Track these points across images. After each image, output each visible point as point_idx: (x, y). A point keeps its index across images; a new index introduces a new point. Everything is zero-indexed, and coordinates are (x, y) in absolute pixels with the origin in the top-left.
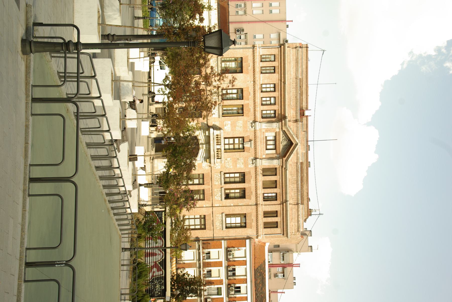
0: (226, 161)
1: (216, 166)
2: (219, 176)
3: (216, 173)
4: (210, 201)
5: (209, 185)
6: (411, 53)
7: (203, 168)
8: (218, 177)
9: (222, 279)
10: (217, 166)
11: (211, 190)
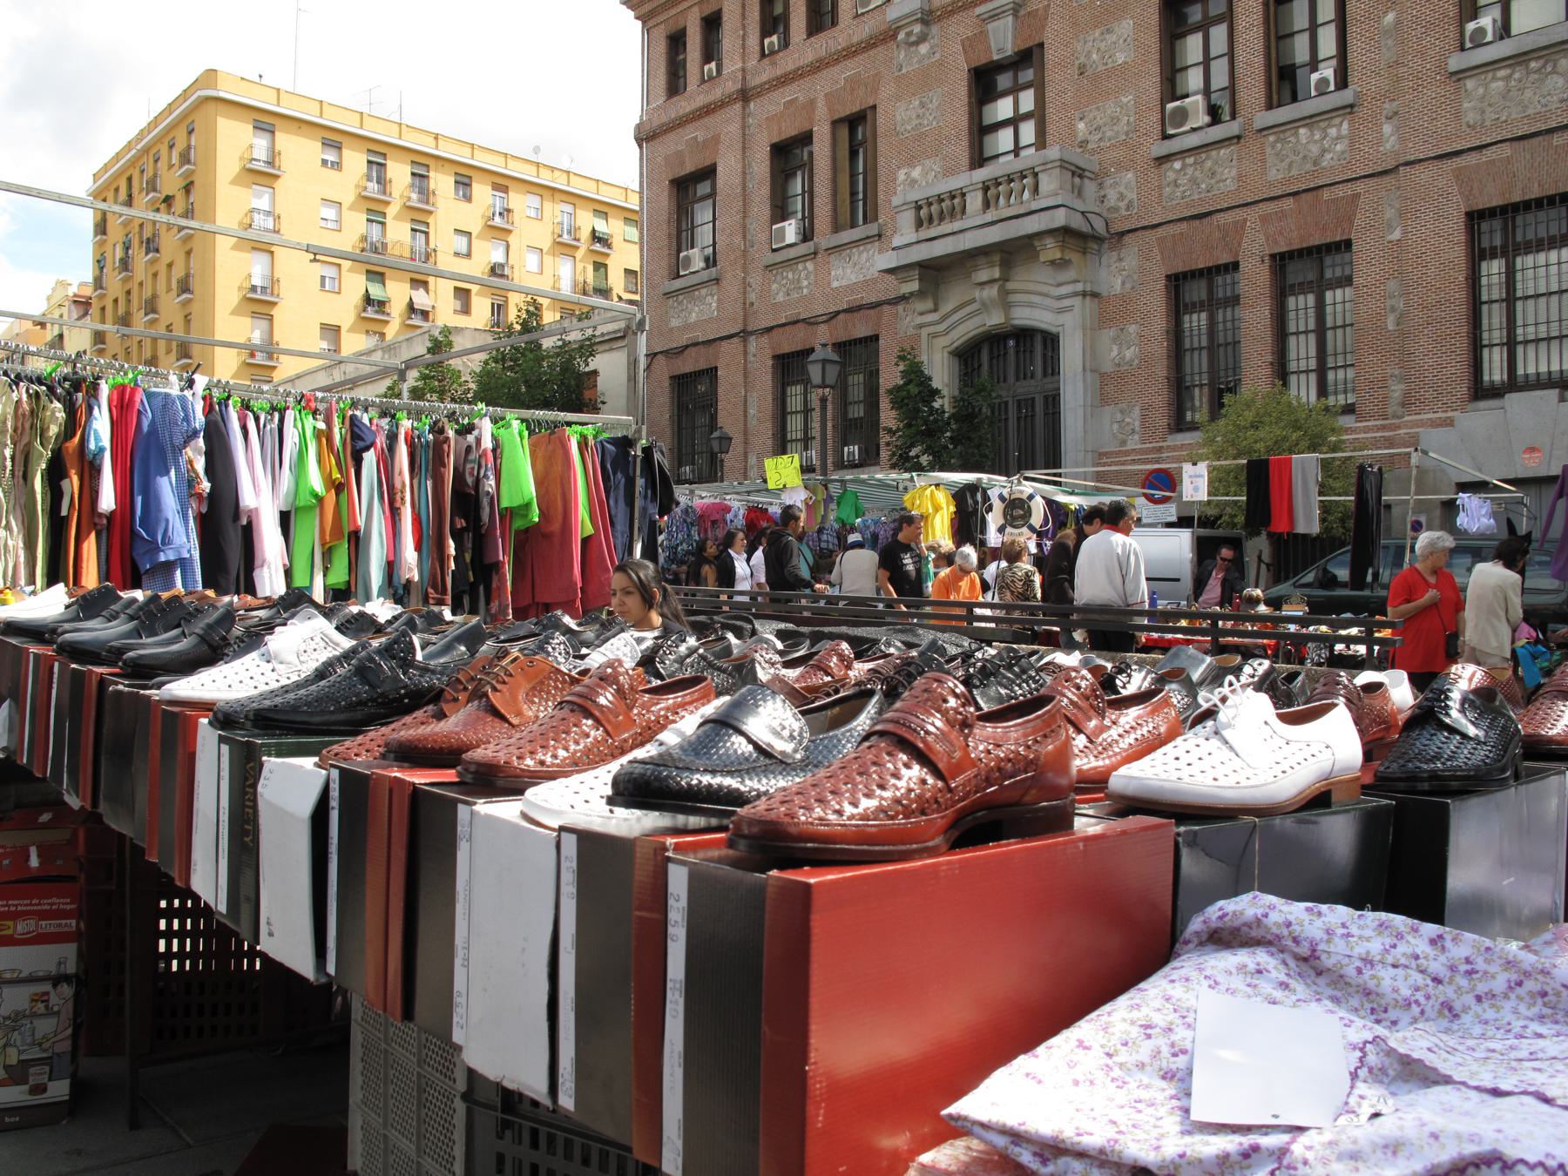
0: (1090, 146)
1: (1122, 204)
5: (1240, 227)
7: (1128, 286)
8: (1190, 171)
10: (1121, 197)
11: (1270, 207)
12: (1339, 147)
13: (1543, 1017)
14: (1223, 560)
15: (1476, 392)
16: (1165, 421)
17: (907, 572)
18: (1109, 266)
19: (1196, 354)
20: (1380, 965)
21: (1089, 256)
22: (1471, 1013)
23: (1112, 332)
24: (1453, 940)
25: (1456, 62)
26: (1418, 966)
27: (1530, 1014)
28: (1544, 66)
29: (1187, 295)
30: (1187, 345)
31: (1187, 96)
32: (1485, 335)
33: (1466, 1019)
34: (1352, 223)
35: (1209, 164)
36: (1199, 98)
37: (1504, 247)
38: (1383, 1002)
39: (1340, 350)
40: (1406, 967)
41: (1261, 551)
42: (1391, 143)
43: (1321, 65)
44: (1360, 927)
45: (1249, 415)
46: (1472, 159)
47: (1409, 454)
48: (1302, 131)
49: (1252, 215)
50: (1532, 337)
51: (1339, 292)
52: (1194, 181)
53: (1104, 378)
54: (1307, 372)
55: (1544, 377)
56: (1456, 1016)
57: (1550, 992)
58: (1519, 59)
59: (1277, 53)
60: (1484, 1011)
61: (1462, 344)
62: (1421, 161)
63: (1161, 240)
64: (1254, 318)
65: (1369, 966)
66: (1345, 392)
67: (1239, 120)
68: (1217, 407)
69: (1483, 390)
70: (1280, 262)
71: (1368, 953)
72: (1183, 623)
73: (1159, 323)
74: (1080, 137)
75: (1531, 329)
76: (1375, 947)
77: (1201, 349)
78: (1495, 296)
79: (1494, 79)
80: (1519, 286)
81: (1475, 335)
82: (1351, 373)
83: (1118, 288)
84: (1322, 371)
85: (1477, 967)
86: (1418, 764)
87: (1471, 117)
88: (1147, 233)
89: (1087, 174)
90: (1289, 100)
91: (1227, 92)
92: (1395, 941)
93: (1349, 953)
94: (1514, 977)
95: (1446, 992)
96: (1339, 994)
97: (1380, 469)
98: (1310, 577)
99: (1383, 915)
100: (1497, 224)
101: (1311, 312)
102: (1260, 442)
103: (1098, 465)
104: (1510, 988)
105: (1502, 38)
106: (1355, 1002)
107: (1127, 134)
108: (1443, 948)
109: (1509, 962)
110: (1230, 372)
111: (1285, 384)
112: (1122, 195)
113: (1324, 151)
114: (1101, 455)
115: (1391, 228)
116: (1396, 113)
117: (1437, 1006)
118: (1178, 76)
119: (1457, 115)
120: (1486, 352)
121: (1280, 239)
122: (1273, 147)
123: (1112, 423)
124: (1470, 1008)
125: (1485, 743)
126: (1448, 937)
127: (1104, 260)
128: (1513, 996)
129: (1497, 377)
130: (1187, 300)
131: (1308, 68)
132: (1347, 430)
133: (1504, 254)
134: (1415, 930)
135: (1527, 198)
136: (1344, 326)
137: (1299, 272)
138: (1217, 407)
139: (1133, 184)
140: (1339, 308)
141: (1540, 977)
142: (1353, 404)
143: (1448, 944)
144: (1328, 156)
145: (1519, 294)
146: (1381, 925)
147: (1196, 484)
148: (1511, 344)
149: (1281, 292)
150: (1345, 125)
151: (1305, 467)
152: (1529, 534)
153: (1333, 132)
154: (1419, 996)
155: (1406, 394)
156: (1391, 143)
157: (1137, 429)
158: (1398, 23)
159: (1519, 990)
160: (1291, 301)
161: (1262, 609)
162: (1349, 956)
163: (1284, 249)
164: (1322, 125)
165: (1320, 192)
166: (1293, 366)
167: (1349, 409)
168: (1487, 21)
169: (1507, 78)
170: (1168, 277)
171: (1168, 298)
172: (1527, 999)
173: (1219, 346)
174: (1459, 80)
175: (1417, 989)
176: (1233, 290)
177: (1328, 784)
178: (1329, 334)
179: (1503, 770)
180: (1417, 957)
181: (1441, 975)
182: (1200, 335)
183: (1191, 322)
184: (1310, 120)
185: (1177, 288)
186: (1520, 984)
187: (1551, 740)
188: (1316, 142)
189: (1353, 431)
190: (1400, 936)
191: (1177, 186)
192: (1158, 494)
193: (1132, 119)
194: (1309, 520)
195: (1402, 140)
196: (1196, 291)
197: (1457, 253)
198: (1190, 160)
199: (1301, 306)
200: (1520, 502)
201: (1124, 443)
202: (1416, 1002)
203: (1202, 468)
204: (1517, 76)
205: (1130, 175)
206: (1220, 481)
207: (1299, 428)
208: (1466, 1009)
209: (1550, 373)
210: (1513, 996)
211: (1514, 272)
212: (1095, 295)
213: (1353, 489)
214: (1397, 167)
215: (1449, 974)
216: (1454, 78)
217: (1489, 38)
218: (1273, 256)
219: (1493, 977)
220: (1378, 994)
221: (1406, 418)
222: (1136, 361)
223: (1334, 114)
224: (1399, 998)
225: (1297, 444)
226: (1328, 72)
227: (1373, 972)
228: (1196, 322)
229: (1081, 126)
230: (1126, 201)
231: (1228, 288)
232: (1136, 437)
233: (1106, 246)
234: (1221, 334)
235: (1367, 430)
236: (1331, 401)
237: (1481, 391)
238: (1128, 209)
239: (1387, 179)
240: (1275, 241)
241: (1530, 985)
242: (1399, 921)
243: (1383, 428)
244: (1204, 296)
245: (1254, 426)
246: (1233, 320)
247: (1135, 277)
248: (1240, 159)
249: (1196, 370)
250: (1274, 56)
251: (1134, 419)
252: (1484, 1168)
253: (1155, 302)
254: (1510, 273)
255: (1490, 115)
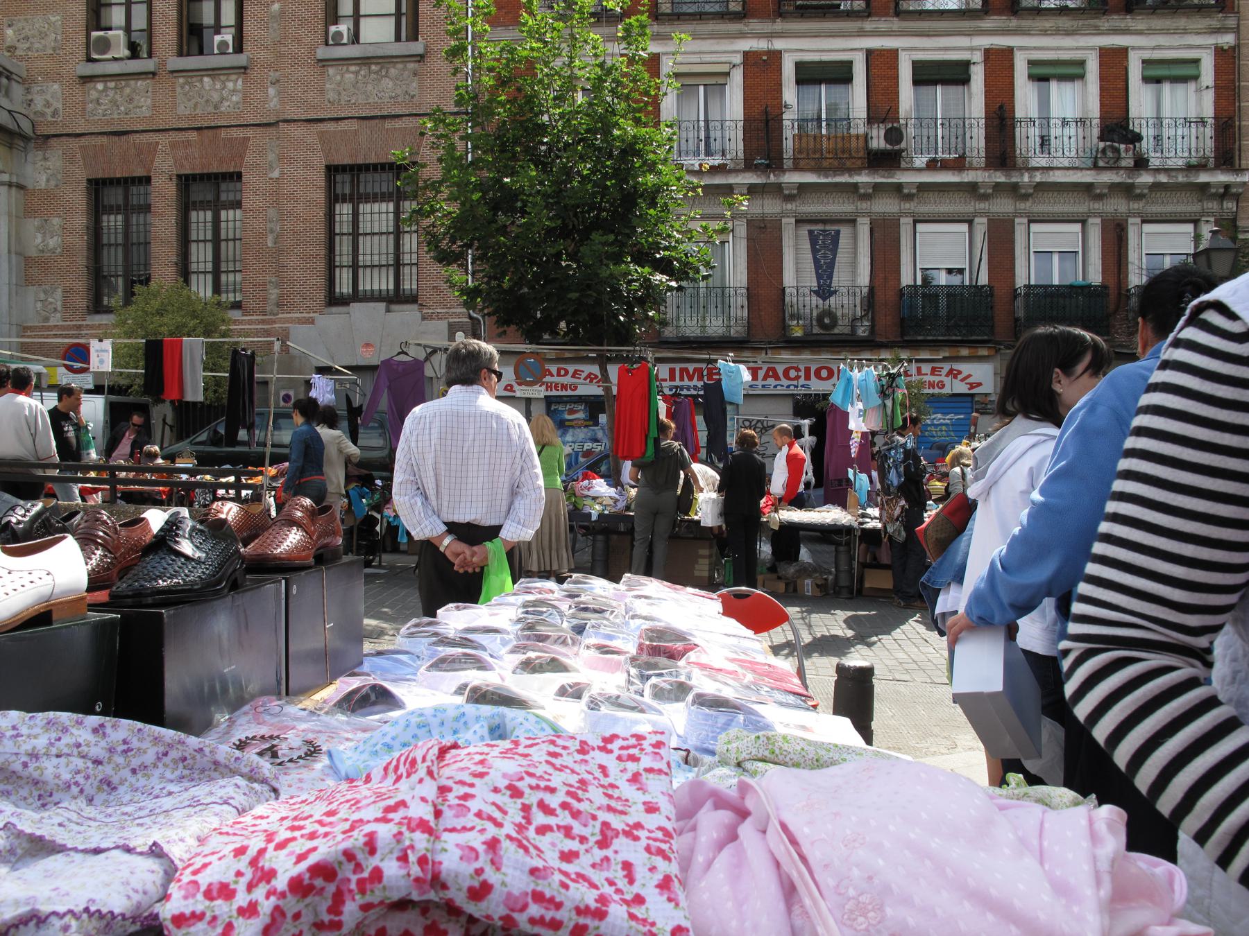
0: (18, 53)
1: (49, 111)
2: (106, 89)
3: (84, 109)
4: (246, 139)
5: (153, 148)
6: (388, 310)
7: (53, 183)
8: (111, 93)
9: (738, 59)
10: (48, 105)
11: (180, 136)
12: (234, 98)
13: (183, 777)
14: (134, 425)
15: (330, 300)
16: (84, 304)
17: (67, 438)
18: (35, 163)
19: (113, 249)
20: (45, 757)
21: (15, 150)
22: (127, 784)
23: (37, 222)
24: (112, 727)
25: (322, 52)
26: (79, 753)
27: (172, 777)
28: (380, 70)
29: (106, 199)
30: (105, 241)
31: (110, 29)
32: (337, 258)
33: (122, 789)
34: (243, 159)
35: (128, 91)
36: (121, 33)
37: (352, 195)
38: (49, 788)
39: (231, 258)
40: (68, 755)
41: (165, 415)
42: (274, 103)
43: (223, 30)
44: (30, 727)
45: (156, 304)
46: (331, 126)
47: (272, 343)
48: (206, 79)
49: (163, 140)
50: (369, 263)
51: (231, 212)
52: (114, 102)
53: (28, 262)
54: (205, 273)
55: (376, 293)
56: (115, 789)
57: (189, 757)
58: (365, 61)
59: (188, 12)
60: (138, 780)
61: (321, 263)
62: (295, 121)
63: (83, 149)
64: (163, 224)
65: (34, 760)
66: (235, 292)
67: (155, 60)
68: (129, 295)
69: (335, 299)
70: (186, 182)
71: (34, 748)
72: (93, 474)
73: (80, 219)
74: (9, 42)
75: (368, 258)
76: (41, 742)
77: (117, 245)
78: (345, 231)
79: (348, 71)
80: (361, 225)
81: (330, 257)
82: (239, 277)
83: (43, 185)
84: (216, 273)
85: (132, 746)
86: (143, 583)
87: (331, 96)
88: (71, 140)
89: (15, 77)
90: (196, 52)
91: (145, 34)
92: (60, 734)
93: (16, 750)
94: (161, 749)
95: (107, 770)
96: (9, 787)
97: (253, 353)
98: (203, 437)
99: (51, 714)
100: (347, 177)
101: (209, 225)
102: (163, 327)
103: (23, 336)
104: (159, 759)
105: (353, 43)
106: (24, 792)
107: (54, 49)
108: (104, 734)
109: (156, 739)
110: (142, 267)
111: (187, 281)
112: (48, 102)
113: (223, 99)
114: (25, 328)
115: (271, 168)
116: (278, 81)
117: (96, 783)
118: (103, 10)
119: (322, 92)
120: (337, 270)
121: (185, 163)
122: (182, 88)
123: (36, 301)
124: (126, 780)
125: (204, 563)
126: (108, 725)
127: (30, 157)
128: (160, 765)
129: (345, 290)
130: (106, 203)
131: (212, 30)
132: (235, 322)
133: (351, 200)
134: (79, 723)
135: (367, 162)
136: (234, 240)
137: (200, 192)
138: (129, 295)
139: (59, 94)
140: (231, 225)
141: (179, 746)
142: (240, 302)
143: (109, 730)
144: (226, 104)
145: (361, 231)
146: (48, 723)
147: (102, 357)
148: (355, 267)
149: (186, 207)
150: (240, 82)
151: (194, 347)
152: (361, 406)
153: (230, 85)
154: (80, 778)
155: (281, 297)
156: (274, 103)
157: (59, 308)
158: (282, 12)
159: (166, 760)
160: (193, 215)
161: (160, 461)
162: (16, 754)
163: (188, 172)
164: (223, 78)
165: (218, 131)
166: (194, 267)
167: (237, 306)
168: (344, 28)
169: (357, 73)
170: (89, 181)
171: (89, 199)
172: (171, 765)
173: (132, 244)
174: (324, 66)
175: (78, 772)
176: (146, 199)
177: (48, 606)
178: (223, 245)
179: (219, 583)
180: (79, 745)
181: (101, 757)
182: (116, 233)
183: (109, 222)
184: (213, 72)
185: (97, 191)
186: (166, 754)
187: (276, 558)
188: (216, 90)
189: (241, 322)
190: (65, 730)
191: (98, 104)
192: (77, 365)
193: (59, 37)
194: (195, 392)
195: (282, 102)
196: (114, 196)
197: (318, 193)
198: (111, 85)
199: (201, 220)
200: (355, 383)
201: (47, 319)
202: (77, 784)
203: (107, 344)
204: (362, 73)
205: (56, 86)
206: (131, 357)
207: (196, 317)
208: (122, 782)
209: (388, 290)
210: (160, 765)
211: (358, 214)
212: (21, 187)
213: (227, 364)
214: (278, 122)
215: (107, 755)
216: (320, 64)
217: (345, 41)
218: (179, 177)
219: (145, 752)
220: (44, 783)
221: (280, 316)
222: (59, 250)
223: (232, 71)
224: (60, 783)
225: (194, 330)
226: (228, 37)
227: (37, 764)
228: (113, 222)
229: (9, 32)
230: (52, 109)
231: (142, 197)
232: (58, 315)
233: (32, 145)
234: (135, 235)
235: (250, 322)
236: (224, 297)
237: (334, 300)
238: (53, 116)
239: (270, 130)
240: (182, 165)
241: (174, 754)
242: (65, 717)
243: (263, 322)
244: (121, 202)
245: (160, 313)
246: (145, 225)
247: (59, 177)
248: (154, 92)
249: (113, 262)
250: (185, 13)
251: (57, 298)
252: (21, 927)
253: (78, 201)
254: (355, 214)
255: (344, 98)
